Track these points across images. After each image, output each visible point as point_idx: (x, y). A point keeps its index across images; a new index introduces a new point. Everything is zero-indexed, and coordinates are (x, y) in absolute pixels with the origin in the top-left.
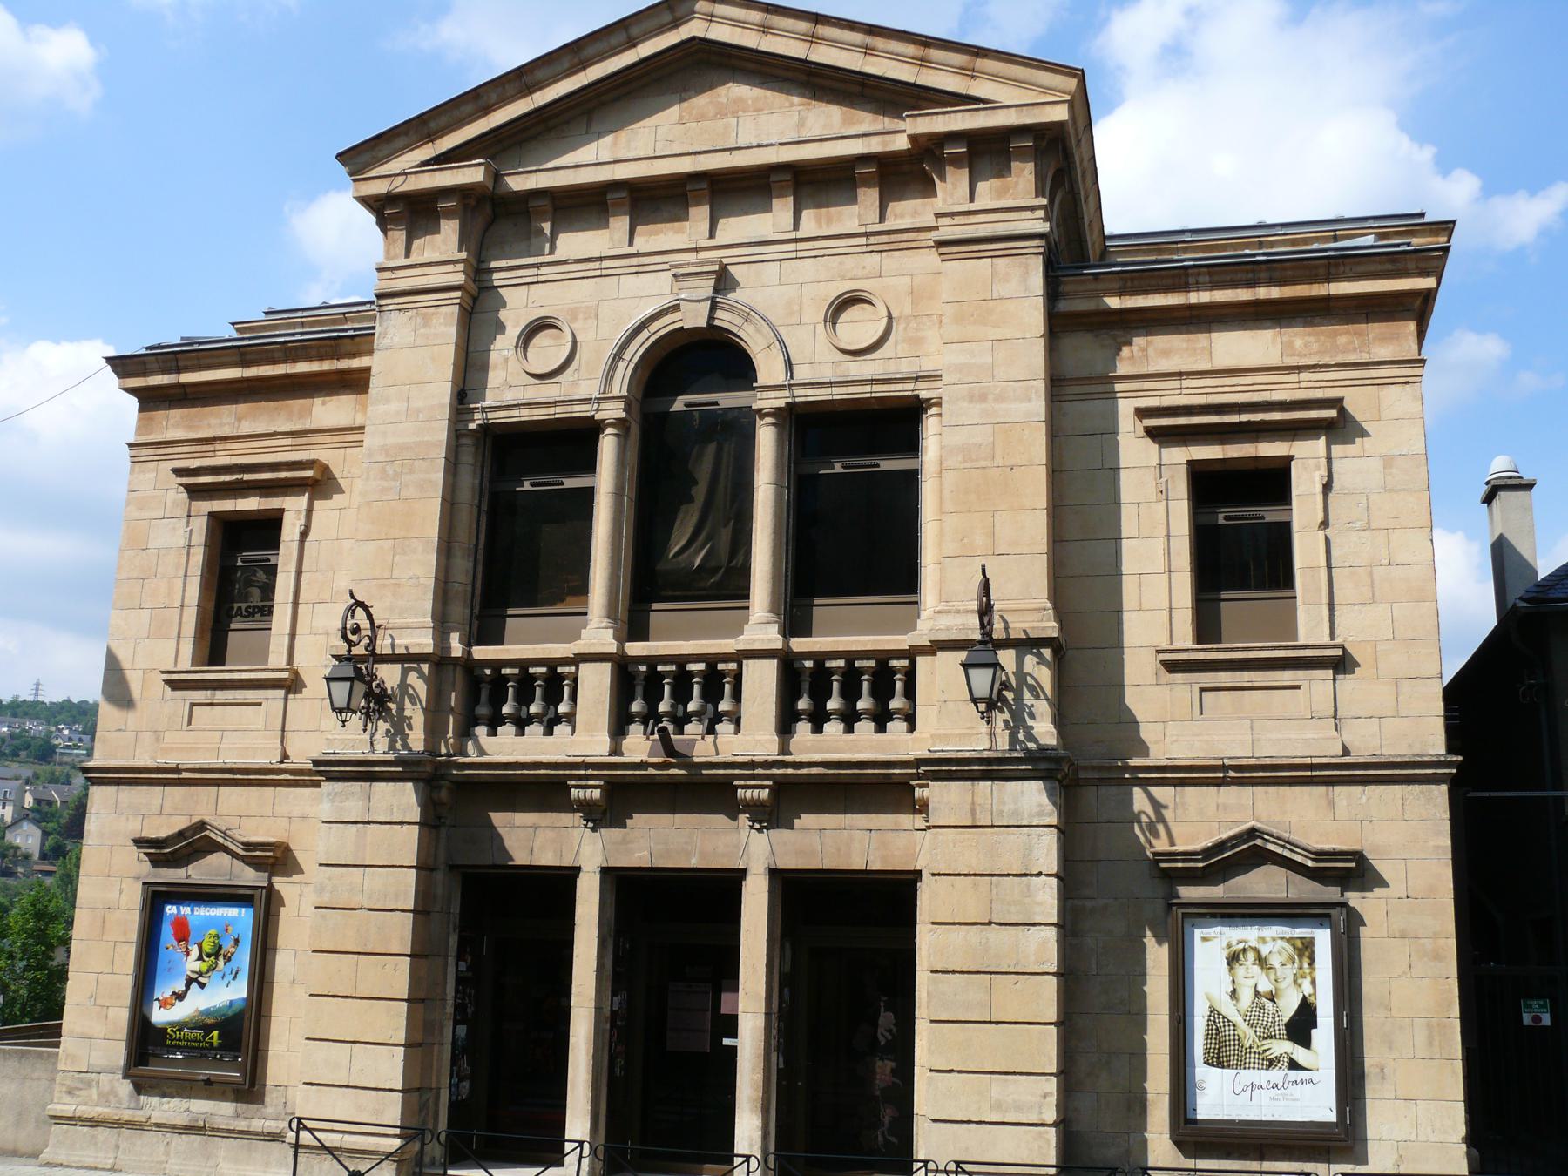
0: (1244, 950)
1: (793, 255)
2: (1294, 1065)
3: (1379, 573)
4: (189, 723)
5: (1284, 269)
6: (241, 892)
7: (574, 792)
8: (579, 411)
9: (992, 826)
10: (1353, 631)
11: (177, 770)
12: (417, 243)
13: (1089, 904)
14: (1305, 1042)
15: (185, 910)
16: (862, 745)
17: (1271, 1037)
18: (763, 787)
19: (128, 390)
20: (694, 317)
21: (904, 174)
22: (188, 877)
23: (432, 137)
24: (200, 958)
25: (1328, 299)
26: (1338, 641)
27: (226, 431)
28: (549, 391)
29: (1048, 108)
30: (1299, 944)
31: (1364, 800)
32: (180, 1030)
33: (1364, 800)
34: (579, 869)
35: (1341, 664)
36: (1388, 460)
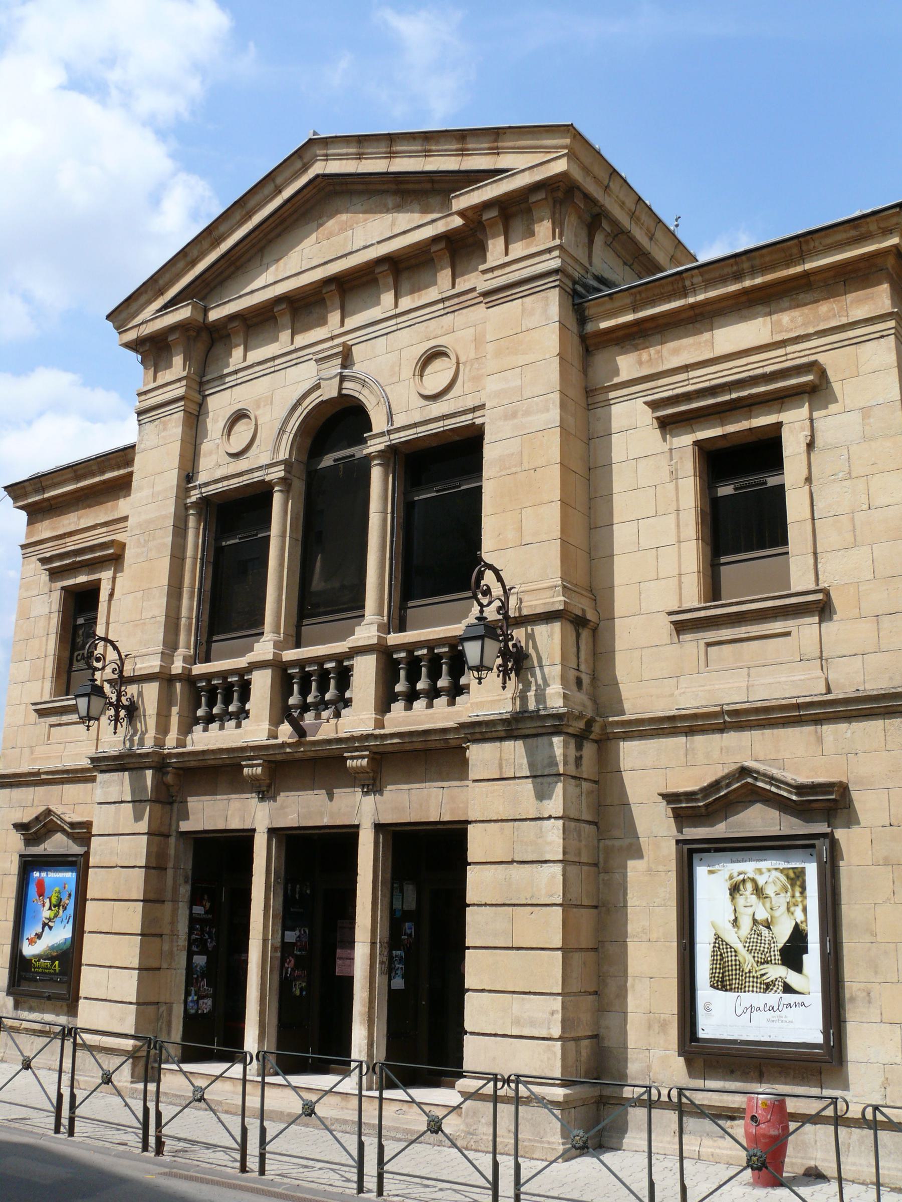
0: (744, 881)
1: (395, 328)
2: (788, 989)
3: (860, 517)
4: (49, 739)
5: (762, 256)
6: (70, 859)
7: (246, 770)
8: (257, 476)
9: (515, 778)
10: (836, 573)
11: (38, 773)
12: (159, 374)
13: (617, 843)
14: (797, 967)
15: (44, 874)
16: (438, 715)
17: (767, 962)
18: (363, 757)
19: (19, 508)
20: (330, 391)
21: (461, 247)
22: (45, 849)
23: (161, 292)
24: (50, 909)
25: (806, 274)
26: (821, 586)
27: (72, 528)
28: (242, 465)
29: (552, 164)
30: (792, 875)
31: (849, 735)
32: (39, 961)
33: (849, 735)
34: (254, 830)
35: (822, 608)
36: (866, 412)
